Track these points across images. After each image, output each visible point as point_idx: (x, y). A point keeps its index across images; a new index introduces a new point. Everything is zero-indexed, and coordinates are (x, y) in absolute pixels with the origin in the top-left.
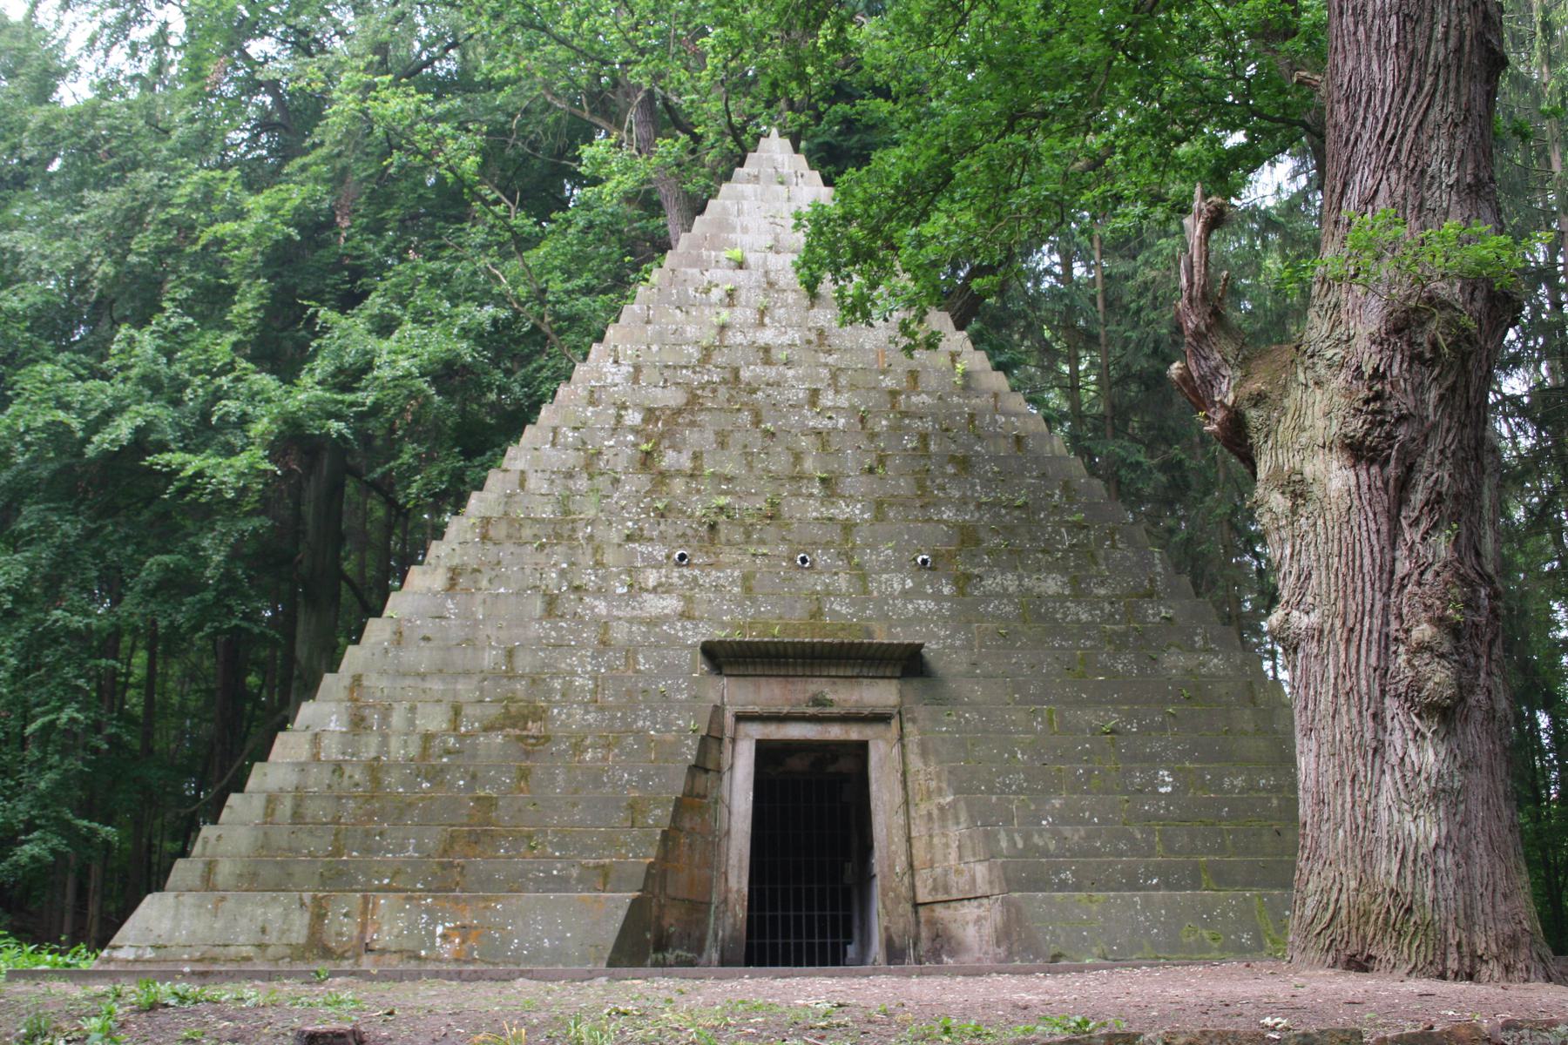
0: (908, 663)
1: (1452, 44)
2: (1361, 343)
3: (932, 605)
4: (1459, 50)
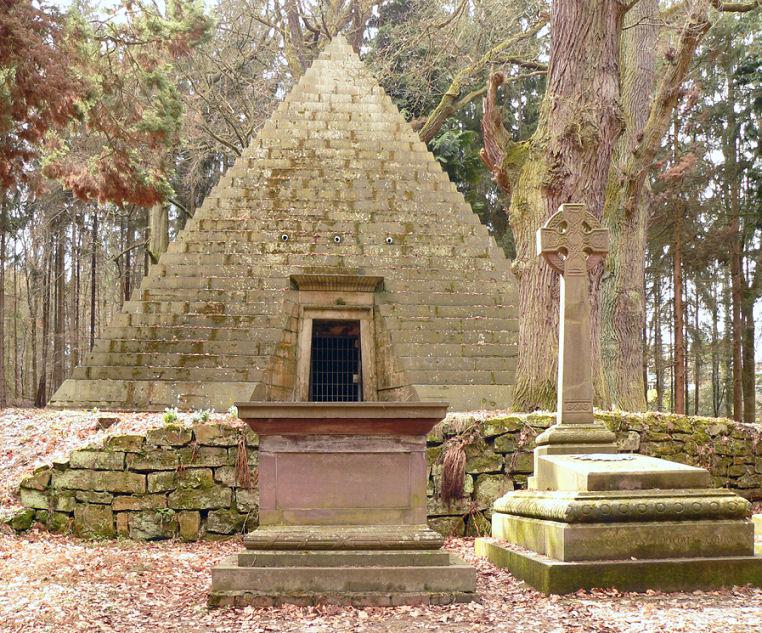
0: (378, 285)
2: (554, 141)
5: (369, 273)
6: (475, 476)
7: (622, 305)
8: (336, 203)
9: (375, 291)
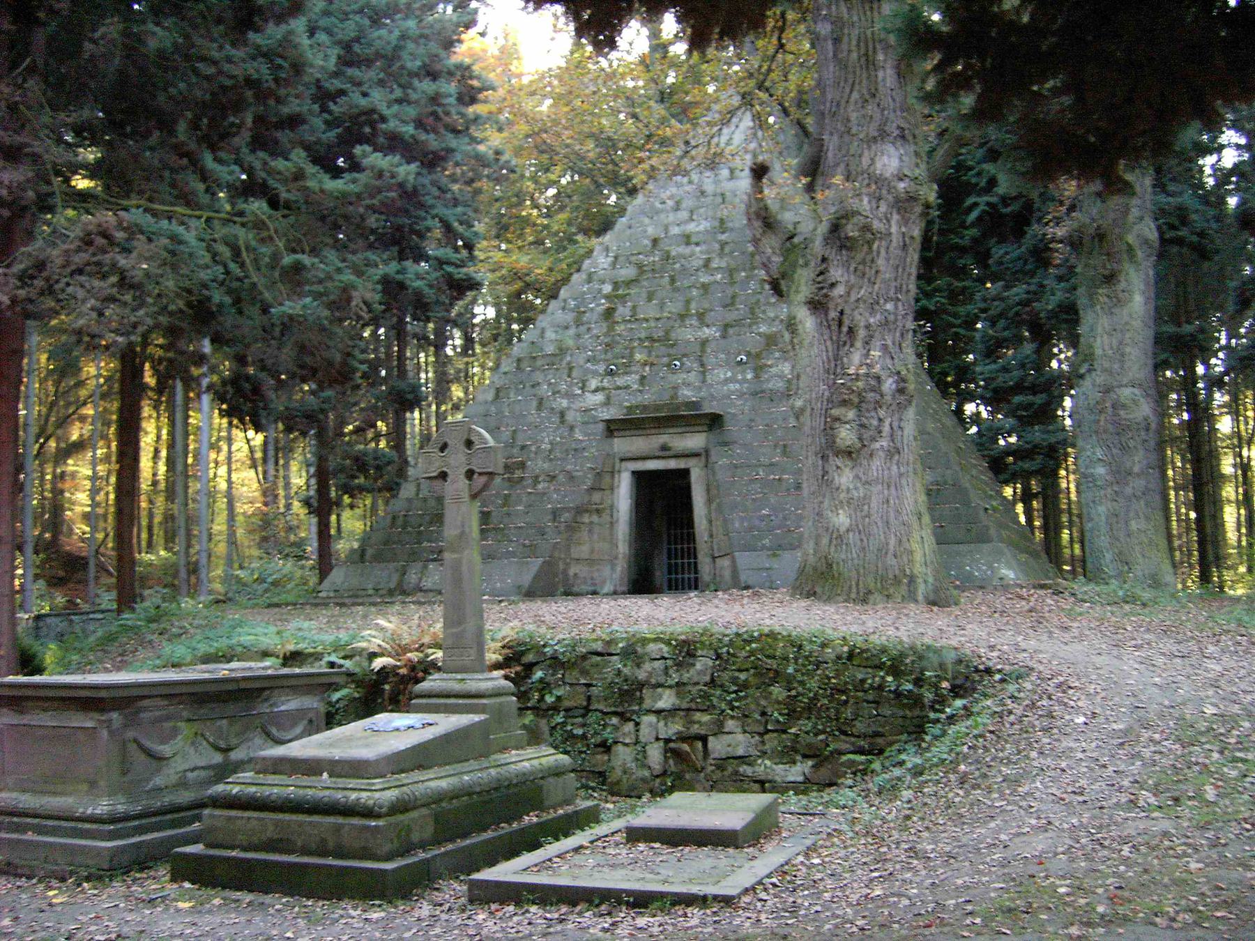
0: (714, 422)
5: (707, 409)
7: (1110, 410)
8: (682, 317)
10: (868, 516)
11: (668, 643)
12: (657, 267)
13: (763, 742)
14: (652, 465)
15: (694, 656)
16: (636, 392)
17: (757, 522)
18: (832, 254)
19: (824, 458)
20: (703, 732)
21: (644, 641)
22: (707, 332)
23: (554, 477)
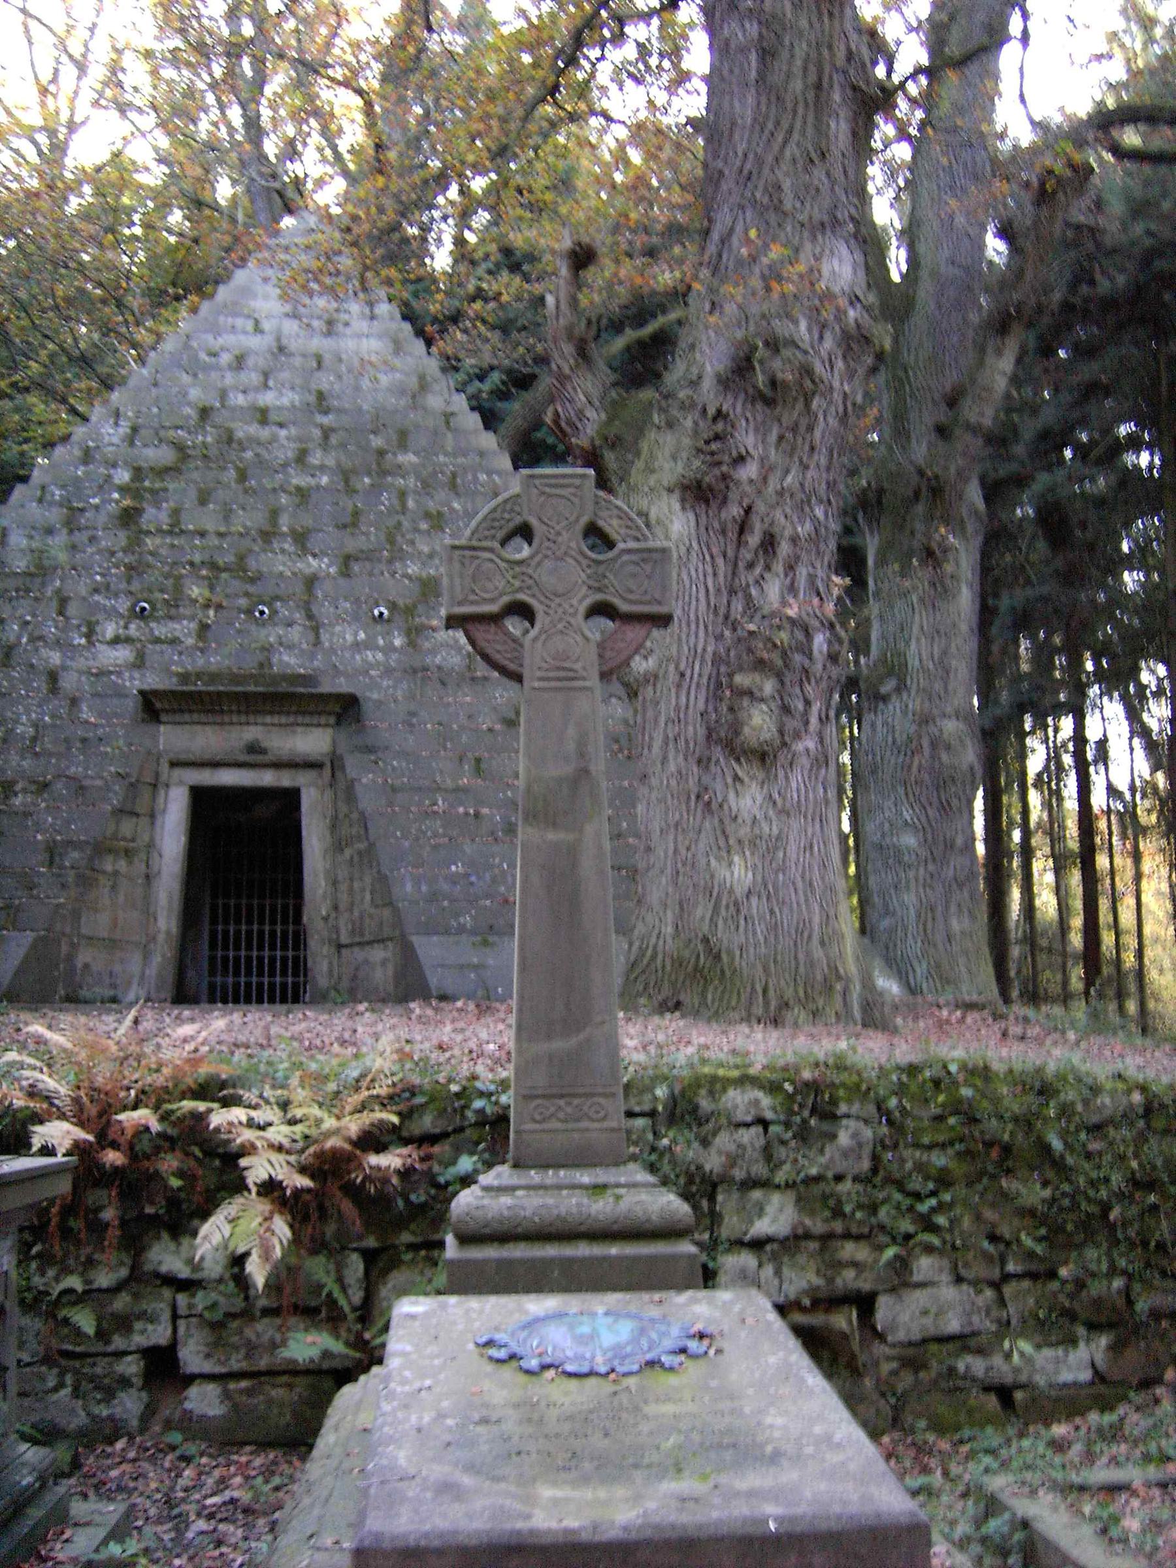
0: (345, 709)
1: (812, 78)
3: (380, 656)
4: (818, 86)
6: (370, 1256)
8: (267, 536)
9: (338, 723)
10: (783, 869)
11: (773, 1088)
12: (213, 452)
13: (1002, 1302)
14: (228, 778)
15: (833, 1117)
16: (182, 651)
17: (445, 887)
18: (734, 406)
19: (703, 762)
20: (866, 1286)
21: (716, 1085)
22: (313, 564)
23: (46, 786)
